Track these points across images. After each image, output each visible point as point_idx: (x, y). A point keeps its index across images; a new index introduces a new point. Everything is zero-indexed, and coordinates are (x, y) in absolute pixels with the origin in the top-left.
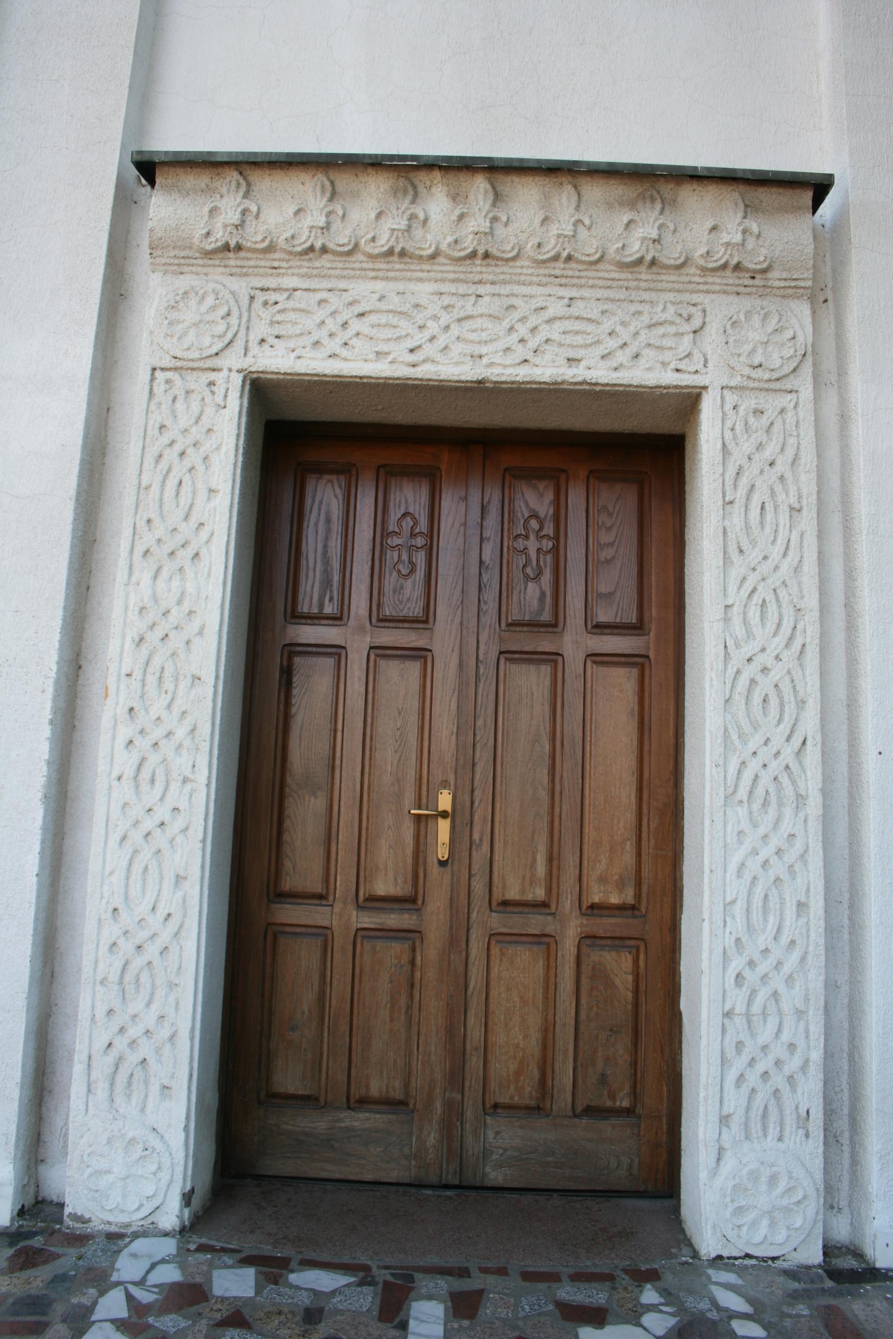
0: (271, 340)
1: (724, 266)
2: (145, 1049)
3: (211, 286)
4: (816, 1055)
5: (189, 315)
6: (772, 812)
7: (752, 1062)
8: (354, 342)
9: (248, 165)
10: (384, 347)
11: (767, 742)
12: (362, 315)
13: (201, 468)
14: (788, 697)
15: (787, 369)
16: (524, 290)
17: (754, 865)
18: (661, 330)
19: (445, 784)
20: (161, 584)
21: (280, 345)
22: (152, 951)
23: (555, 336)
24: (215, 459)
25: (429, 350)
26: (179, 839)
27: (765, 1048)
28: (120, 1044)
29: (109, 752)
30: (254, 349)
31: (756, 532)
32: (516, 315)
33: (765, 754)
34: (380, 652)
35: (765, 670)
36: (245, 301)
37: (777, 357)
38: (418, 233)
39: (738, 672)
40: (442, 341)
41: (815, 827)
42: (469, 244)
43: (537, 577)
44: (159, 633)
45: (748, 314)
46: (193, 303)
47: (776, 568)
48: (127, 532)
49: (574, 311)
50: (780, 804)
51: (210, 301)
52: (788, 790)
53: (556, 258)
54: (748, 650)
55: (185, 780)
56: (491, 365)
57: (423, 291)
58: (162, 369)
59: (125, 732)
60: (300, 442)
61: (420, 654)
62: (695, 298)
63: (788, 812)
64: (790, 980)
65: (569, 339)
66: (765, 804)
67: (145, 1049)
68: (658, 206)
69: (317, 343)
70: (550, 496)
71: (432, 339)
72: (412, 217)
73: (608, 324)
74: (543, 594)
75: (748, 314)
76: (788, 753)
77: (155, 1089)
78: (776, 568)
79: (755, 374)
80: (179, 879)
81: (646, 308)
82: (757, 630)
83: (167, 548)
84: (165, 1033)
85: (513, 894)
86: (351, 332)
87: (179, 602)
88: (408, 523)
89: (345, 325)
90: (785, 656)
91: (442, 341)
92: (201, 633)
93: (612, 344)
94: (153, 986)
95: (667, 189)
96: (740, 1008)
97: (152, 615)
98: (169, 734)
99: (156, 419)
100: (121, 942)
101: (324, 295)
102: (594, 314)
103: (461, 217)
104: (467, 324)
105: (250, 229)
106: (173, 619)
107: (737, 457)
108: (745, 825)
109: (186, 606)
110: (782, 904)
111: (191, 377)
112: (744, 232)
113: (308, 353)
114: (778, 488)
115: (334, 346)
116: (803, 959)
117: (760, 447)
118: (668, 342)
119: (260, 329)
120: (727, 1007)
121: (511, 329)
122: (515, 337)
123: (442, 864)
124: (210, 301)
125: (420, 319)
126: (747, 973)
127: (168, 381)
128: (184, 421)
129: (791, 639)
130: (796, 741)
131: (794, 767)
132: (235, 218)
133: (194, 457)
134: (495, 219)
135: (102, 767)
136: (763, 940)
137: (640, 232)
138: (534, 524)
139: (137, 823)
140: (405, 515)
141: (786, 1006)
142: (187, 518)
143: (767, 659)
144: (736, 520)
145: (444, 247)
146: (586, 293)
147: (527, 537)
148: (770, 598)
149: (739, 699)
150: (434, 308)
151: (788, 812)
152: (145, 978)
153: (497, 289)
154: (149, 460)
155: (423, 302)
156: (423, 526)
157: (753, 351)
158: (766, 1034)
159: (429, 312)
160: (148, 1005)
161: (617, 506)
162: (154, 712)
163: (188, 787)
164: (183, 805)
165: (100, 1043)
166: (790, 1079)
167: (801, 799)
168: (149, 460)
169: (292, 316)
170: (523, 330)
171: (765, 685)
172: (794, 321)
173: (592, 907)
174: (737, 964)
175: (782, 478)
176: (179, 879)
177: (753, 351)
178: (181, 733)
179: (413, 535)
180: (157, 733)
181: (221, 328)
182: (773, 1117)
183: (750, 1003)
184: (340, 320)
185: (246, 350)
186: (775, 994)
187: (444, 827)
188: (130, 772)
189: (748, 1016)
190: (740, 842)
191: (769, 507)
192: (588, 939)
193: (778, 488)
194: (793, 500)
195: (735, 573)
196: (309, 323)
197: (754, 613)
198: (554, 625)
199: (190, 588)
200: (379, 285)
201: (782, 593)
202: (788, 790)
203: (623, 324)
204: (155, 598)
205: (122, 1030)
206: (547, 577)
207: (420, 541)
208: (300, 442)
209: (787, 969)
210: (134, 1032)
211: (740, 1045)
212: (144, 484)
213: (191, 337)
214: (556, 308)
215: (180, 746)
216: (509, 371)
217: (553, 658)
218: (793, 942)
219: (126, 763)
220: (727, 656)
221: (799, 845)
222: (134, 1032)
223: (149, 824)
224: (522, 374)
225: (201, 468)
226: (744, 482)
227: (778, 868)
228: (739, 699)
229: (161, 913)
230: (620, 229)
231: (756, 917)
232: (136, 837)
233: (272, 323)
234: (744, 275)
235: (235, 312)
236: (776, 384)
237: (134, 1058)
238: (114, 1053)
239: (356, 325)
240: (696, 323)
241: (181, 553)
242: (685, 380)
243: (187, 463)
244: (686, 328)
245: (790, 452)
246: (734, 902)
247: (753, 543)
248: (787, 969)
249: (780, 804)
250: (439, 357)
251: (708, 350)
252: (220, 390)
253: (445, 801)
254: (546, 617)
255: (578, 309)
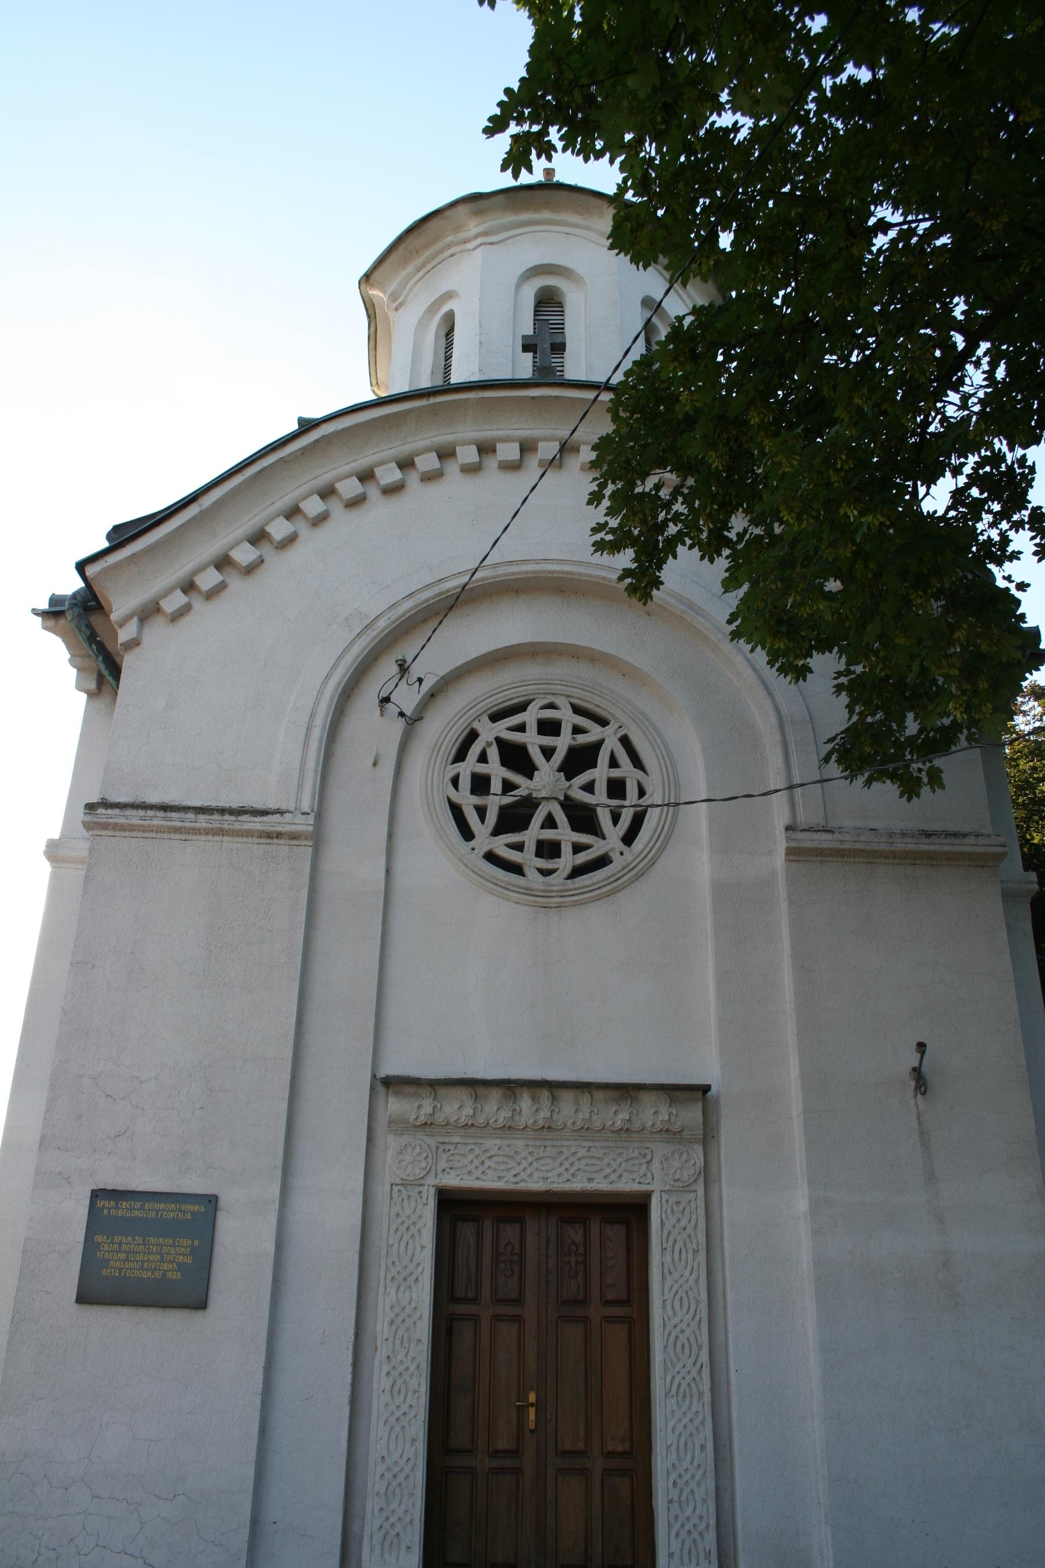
0: (448, 1170)
1: (661, 1130)
2: (399, 1527)
3: (418, 1142)
4: (713, 1522)
5: (408, 1158)
6: (687, 1401)
7: (683, 1525)
8: (487, 1171)
9: (435, 1085)
10: (501, 1174)
11: (684, 1366)
12: (491, 1157)
13: (417, 1236)
14: (694, 1345)
15: (691, 1181)
16: (567, 1143)
17: (680, 1427)
18: (632, 1162)
19: (532, 1388)
20: (400, 1294)
21: (453, 1173)
22: (401, 1477)
23: (582, 1167)
24: (424, 1231)
25: (523, 1176)
26: (413, 1421)
27: (688, 1518)
28: (387, 1525)
29: (379, 1379)
30: (440, 1175)
31: (677, 1263)
32: (563, 1157)
33: (683, 1372)
34: (497, 1318)
35: (682, 1331)
36: (434, 1150)
37: (687, 1175)
38: (517, 1117)
39: (670, 1333)
40: (529, 1171)
41: (708, 1408)
42: (541, 1123)
43: (577, 1274)
44: (400, 1319)
45: (673, 1154)
46: (409, 1150)
47: (687, 1281)
48: (383, 1268)
49: (591, 1154)
50: (691, 1396)
51: (418, 1150)
52: (695, 1389)
53: (582, 1128)
54: (674, 1322)
55: (415, 1392)
56: (552, 1182)
57: (520, 1143)
58: (397, 1185)
59: (386, 1368)
60: (455, 1208)
61: (518, 1319)
62: (648, 1145)
63: (695, 1400)
64: (698, 1484)
65: (588, 1168)
66: (684, 1396)
67: (399, 1527)
68: (629, 1102)
69: (470, 1172)
70: (581, 1232)
71: (524, 1169)
72: (514, 1110)
73: (606, 1161)
74: (579, 1285)
75: (673, 1154)
76: (694, 1373)
77: (403, 1548)
78: (687, 1281)
79: (678, 1184)
80: (414, 1441)
81: (625, 1151)
82: (678, 1312)
83: (403, 1276)
84: (408, 1519)
85: (567, 1447)
86: (486, 1166)
87: (410, 1303)
88: (510, 1248)
89: (483, 1163)
90: (692, 1324)
91: (529, 1171)
92: (420, 1318)
93: (608, 1170)
94: (402, 1496)
95: (633, 1093)
96: (676, 1498)
97: (396, 1310)
98: (407, 1369)
99: (394, 1211)
100: (386, 1474)
101: (472, 1147)
102: (600, 1155)
103: (537, 1110)
104: (541, 1162)
105: (437, 1116)
106: (407, 1310)
107: (668, 1227)
108: (675, 1407)
109: (413, 1305)
110: (694, 1446)
111: (410, 1188)
112: (669, 1114)
113: (465, 1177)
114: (688, 1241)
115: (478, 1173)
116: (704, 1473)
117: (679, 1221)
118: (635, 1169)
119: (443, 1164)
120: (670, 1497)
121: (561, 1164)
122: (563, 1168)
123: (532, 1431)
124: (418, 1150)
125: (518, 1159)
126: (678, 1481)
127: (399, 1191)
128: (408, 1212)
129: (695, 1315)
130: (698, 1366)
131: (697, 1378)
132: (430, 1111)
133: (414, 1230)
134: (553, 1111)
135: (375, 1385)
136: (686, 1464)
137: (620, 1116)
138: (573, 1247)
139: (392, 1413)
140: (508, 1243)
141: (698, 1498)
142: (411, 1261)
143: (683, 1326)
144: (668, 1258)
145: (529, 1124)
146: (596, 1144)
147: (570, 1255)
148: (684, 1295)
149: (670, 1345)
150: (524, 1154)
151: (695, 1400)
152: (398, 1491)
153: (554, 1143)
154: (392, 1231)
155: (520, 1150)
156: (517, 1249)
157: (675, 1172)
158: (688, 1511)
159: (522, 1156)
160: (400, 1505)
161: (616, 1233)
162: (399, 1358)
163: (417, 1395)
164: (414, 1404)
165: (376, 1526)
166: (701, 1533)
167: (701, 1394)
168: (392, 1231)
169: (457, 1157)
170: (567, 1164)
171: (683, 1338)
172: (694, 1156)
173: (609, 1453)
174: (673, 1476)
175: (689, 1235)
176: (414, 1441)
177: (675, 1172)
178: (412, 1368)
179: (512, 1255)
180: (401, 1368)
181: (424, 1164)
182: (694, 1554)
183: (680, 1495)
184: (480, 1160)
185: (436, 1174)
186: (692, 1491)
187: (532, 1411)
188: (388, 1387)
189: (680, 1501)
190: (673, 1416)
191: (683, 1250)
192: (608, 1471)
193: (688, 1241)
194: (694, 1246)
195: (667, 1284)
196: (466, 1162)
197: (677, 1304)
198: (584, 1302)
199: (414, 1296)
200: (498, 1142)
201: (690, 1293)
202: (695, 1389)
203: (614, 1159)
204: (398, 1300)
205: (387, 1518)
206: (581, 1277)
207: (515, 1258)
208: (455, 1208)
209: (697, 1478)
210: (393, 1519)
211: (676, 1517)
212: (390, 1243)
213: (409, 1169)
214: (582, 1153)
215: (412, 1375)
216: (561, 1186)
217: (585, 1320)
218: (699, 1465)
219: (386, 1383)
220: (664, 1325)
221: (700, 1416)
222: (393, 1519)
223: (398, 1414)
224: (567, 1187)
225: (417, 1236)
226: (671, 1238)
227: (691, 1428)
228: (670, 1345)
229: (405, 1458)
230: (611, 1115)
231: (682, 1452)
232: (392, 1420)
233: (448, 1161)
234: (670, 1134)
235: (430, 1156)
236: (687, 1188)
237: (393, 1533)
238: (383, 1531)
239: (488, 1163)
240: (649, 1157)
241: (409, 1279)
242: (644, 1188)
243: (410, 1233)
244: (643, 1161)
245: (693, 1222)
246: (671, 1445)
247: (676, 1269)
248: (697, 1478)
249: (691, 1396)
250: (528, 1179)
251: (654, 1171)
252: (424, 1196)
253: (532, 1397)
254: (581, 1297)
255: (594, 1152)
